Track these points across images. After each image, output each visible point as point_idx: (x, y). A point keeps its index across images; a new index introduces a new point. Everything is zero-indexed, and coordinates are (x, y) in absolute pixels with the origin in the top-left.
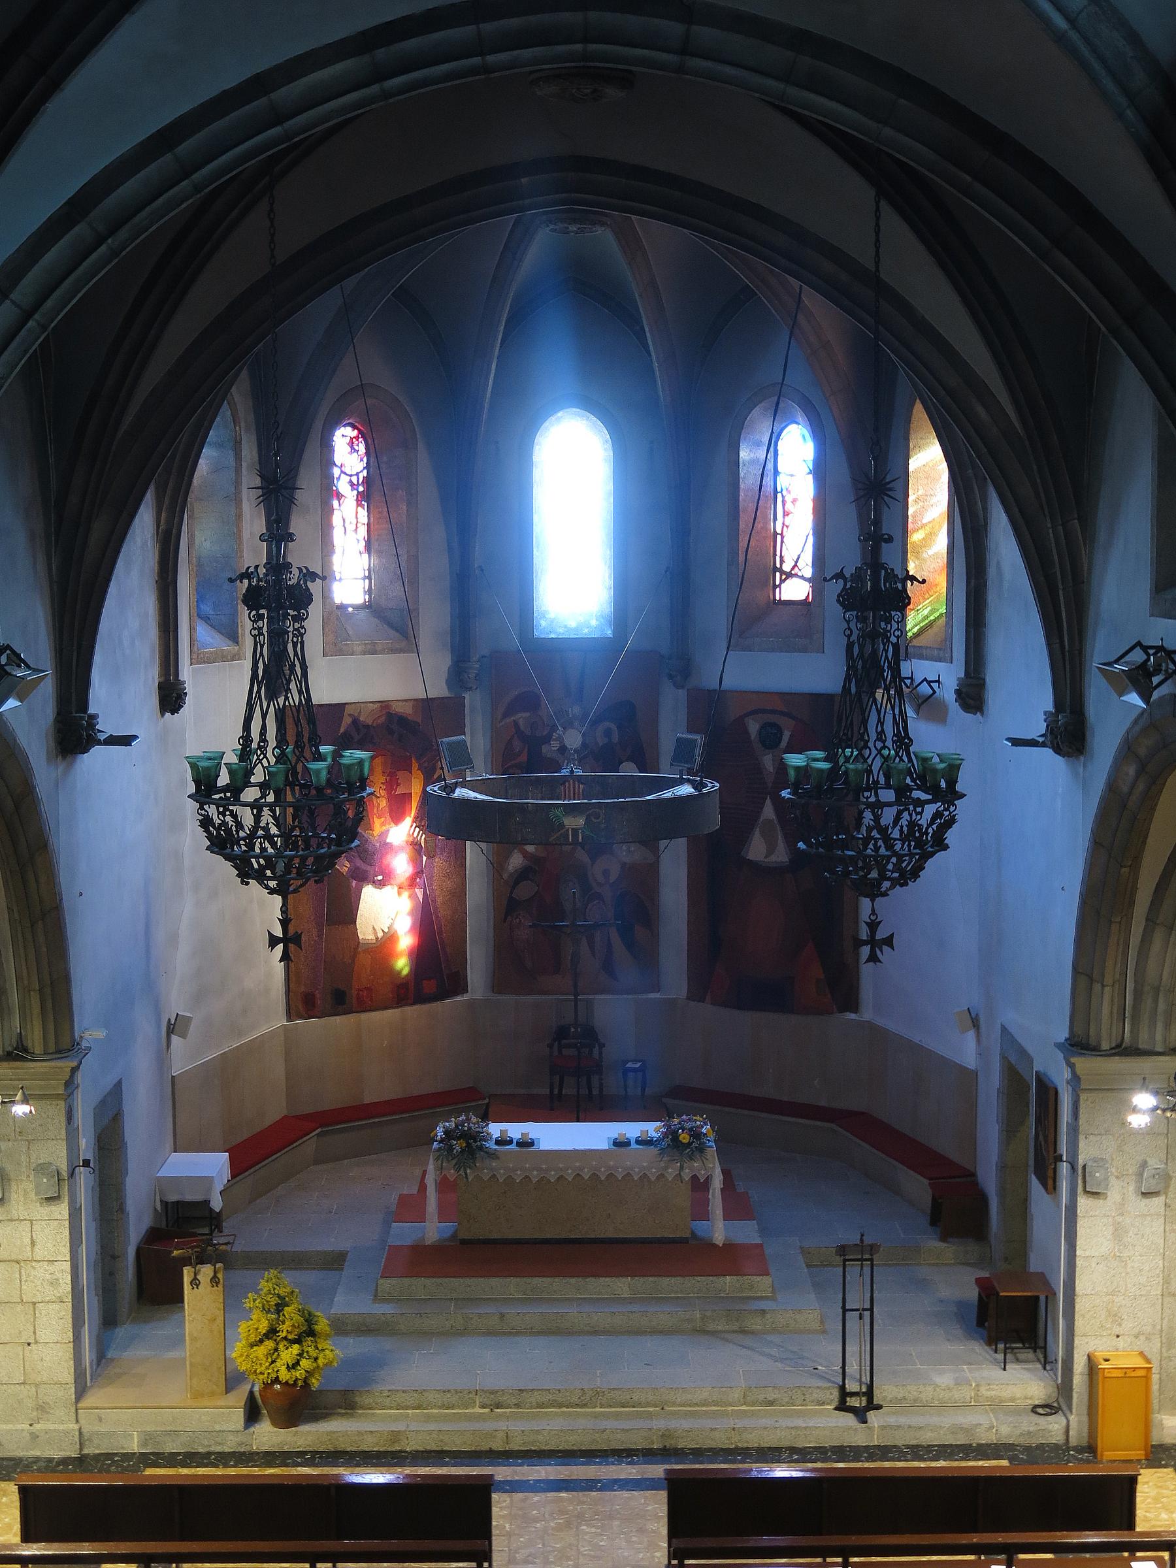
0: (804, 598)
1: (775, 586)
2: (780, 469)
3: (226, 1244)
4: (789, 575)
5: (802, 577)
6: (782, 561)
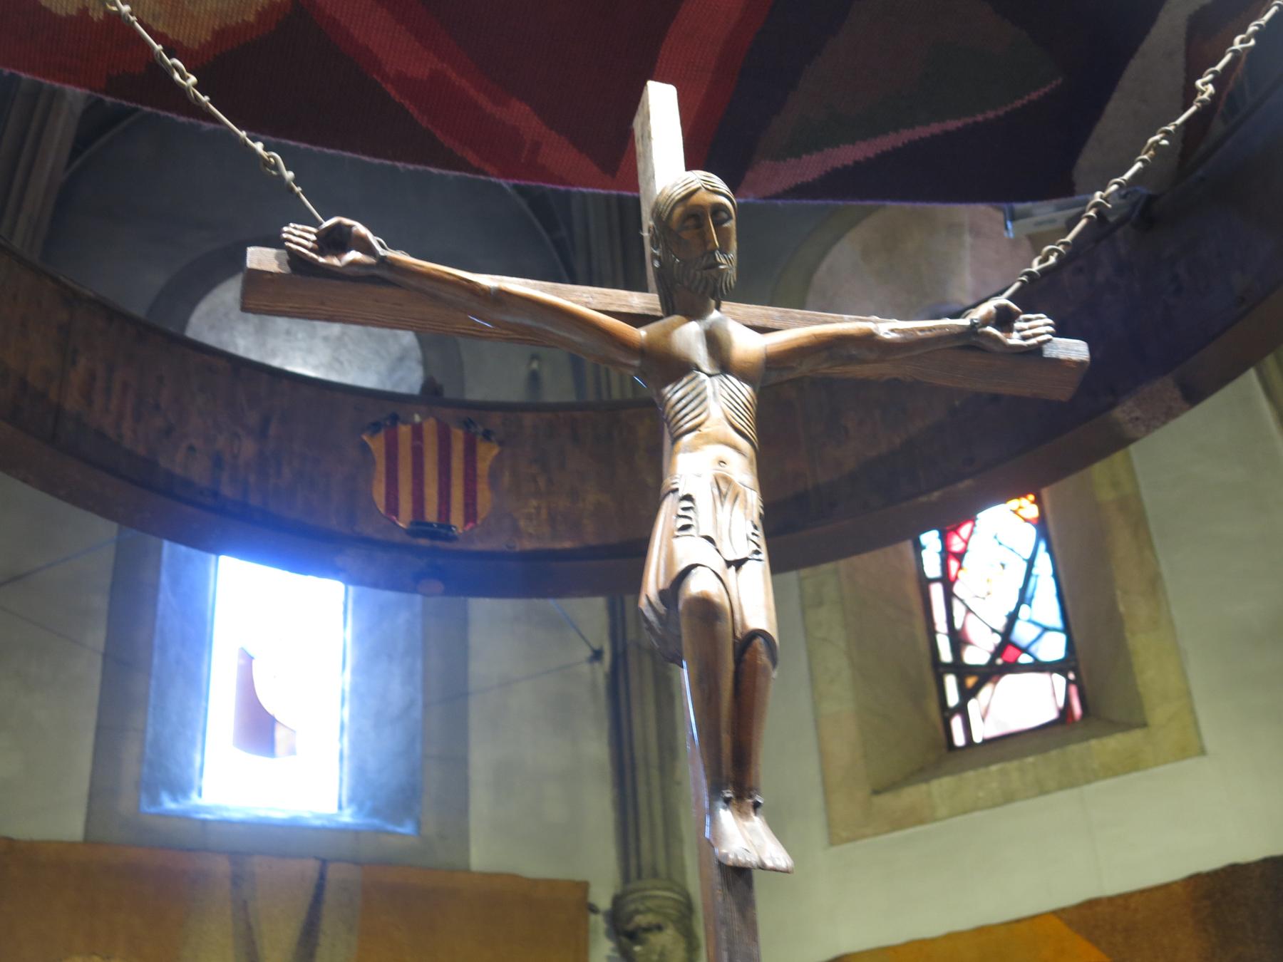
0: (1052, 715)
1: (947, 713)
2: (1024, 566)
3: (181, 21)
4: (990, 673)
5: (1039, 667)
6: (959, 640)
